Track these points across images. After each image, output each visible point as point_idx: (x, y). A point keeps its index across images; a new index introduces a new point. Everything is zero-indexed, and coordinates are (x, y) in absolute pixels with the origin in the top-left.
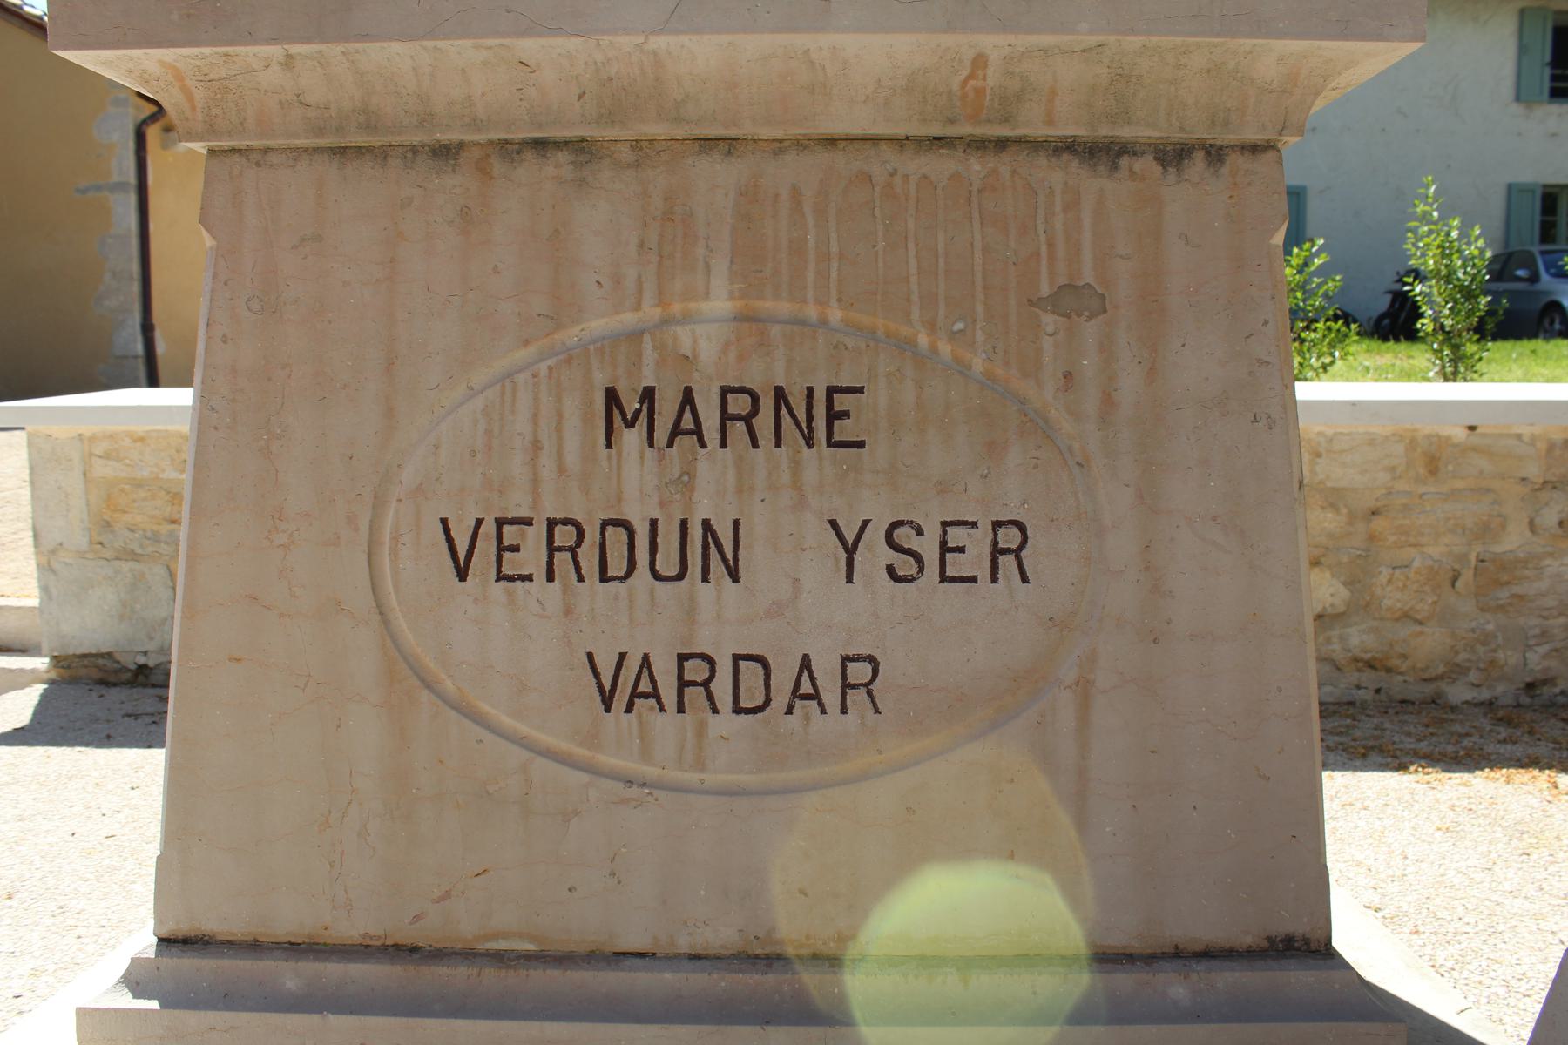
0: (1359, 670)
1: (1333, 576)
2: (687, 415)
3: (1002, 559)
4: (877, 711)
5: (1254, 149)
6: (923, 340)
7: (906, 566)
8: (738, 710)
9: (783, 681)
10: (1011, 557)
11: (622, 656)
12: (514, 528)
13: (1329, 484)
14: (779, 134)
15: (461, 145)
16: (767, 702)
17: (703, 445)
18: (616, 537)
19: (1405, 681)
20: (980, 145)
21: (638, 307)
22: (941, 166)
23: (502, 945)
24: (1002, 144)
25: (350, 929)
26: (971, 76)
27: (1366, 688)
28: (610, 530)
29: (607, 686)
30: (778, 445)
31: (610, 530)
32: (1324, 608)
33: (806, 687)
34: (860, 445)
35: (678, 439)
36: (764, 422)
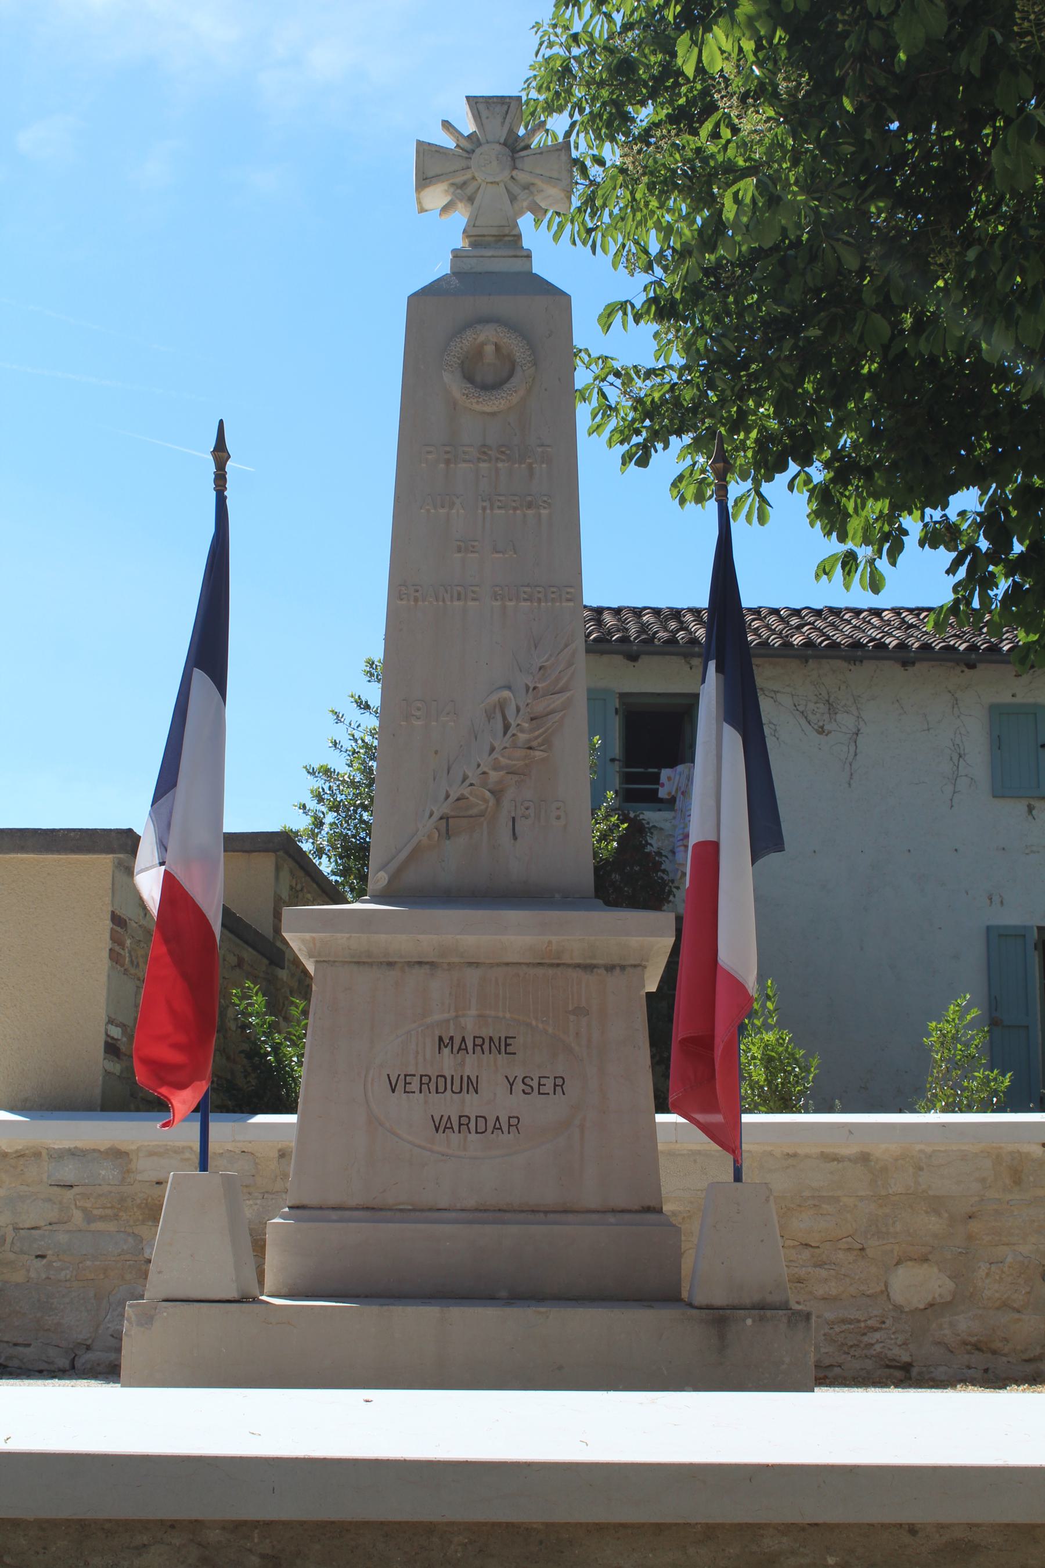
0: (969, 1353)
1: (940, 1270)
2: (463, 1044)
3: (557, 1088)
4: (519, 1133)
5: (635, 966)
6: (534, 1023)
7: (528, 1089)
8: (477, 1132)
9: (491, 1125)
10: (560, 1087)
11: (442, 1116)
12: (410, 1077)
13: (931, 1193)
14: (491, 961)
15: (396, 963)
16: (486, 1130)
17: (468, 1053)
18: (441, 1080)
19: (1009, 1362)
20: (552, 965)
21: (449, 1012)
22: (540, 971)
23: (401, 1207)
24: (558, 965)
25: (353, 1202)
26: (548, 946)
27: (975, 1368)
28: (439, 1078)
29: (437, 1126)
30: (490, 1053)
31: (439, 1078)
32: (934, 1298)
33: (498, 1126)
34: (515, 1054)
35: (460, 1052)
36: (486, 1047)
